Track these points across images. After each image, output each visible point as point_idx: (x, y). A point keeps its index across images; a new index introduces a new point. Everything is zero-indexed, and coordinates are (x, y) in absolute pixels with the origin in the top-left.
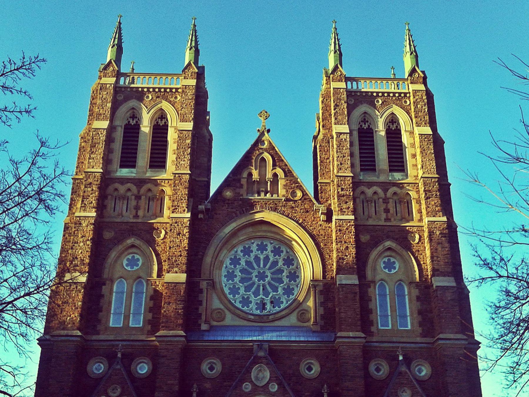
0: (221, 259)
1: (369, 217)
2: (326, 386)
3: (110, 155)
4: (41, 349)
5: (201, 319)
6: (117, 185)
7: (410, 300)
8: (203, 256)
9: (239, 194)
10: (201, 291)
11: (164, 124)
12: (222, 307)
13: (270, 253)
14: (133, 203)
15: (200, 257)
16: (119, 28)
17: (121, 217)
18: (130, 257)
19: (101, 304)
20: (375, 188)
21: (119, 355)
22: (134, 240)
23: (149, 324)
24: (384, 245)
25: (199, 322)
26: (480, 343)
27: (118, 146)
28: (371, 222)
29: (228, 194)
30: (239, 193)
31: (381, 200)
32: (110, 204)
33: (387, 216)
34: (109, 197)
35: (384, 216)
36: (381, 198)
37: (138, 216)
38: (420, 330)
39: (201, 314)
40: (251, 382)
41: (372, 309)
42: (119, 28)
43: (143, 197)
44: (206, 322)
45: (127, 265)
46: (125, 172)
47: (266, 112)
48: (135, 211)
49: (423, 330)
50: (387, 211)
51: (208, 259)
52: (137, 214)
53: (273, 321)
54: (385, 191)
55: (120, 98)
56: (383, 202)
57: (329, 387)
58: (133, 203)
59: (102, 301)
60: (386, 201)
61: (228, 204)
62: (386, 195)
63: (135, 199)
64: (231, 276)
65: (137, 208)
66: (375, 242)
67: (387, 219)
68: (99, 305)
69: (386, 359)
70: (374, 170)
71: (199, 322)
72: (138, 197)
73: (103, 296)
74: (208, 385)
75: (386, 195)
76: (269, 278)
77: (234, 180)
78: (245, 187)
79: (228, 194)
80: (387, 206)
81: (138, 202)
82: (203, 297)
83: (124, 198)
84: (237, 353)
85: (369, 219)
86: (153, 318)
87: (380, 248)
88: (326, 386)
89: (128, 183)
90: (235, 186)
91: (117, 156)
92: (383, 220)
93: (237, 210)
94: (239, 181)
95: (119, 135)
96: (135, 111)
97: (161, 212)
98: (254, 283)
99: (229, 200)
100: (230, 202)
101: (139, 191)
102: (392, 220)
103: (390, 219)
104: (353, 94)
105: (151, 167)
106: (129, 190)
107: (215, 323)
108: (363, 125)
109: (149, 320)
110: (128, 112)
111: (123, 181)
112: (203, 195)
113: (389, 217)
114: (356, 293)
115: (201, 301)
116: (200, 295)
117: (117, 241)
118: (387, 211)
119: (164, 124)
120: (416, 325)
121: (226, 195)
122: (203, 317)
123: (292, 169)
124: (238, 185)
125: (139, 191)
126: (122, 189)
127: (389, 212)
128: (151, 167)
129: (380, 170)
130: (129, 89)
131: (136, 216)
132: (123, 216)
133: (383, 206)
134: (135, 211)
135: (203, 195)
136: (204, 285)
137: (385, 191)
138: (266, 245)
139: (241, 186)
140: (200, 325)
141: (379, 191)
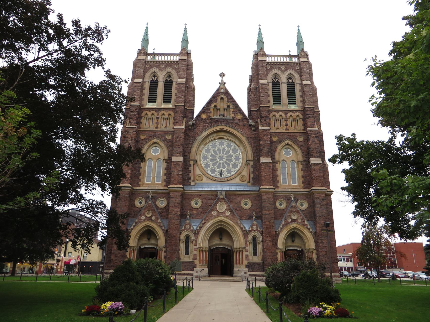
6: (147, 112)
7: (298, 170)
8: (191, 148)
10: (190, 166)
15: (189, 148)
18: (154, 148)
27: (146, 92)
32: (143, 121)
33: (287, 127)
34: (143, 118)
35: (285, 127)
39: (191, 177)
43: (160, 118)
44: (194, 181)
45: (153, 152)
46: (150, 105)
50: (287, 125)
51: (194, 150)
52: (157, 126)
54: (286, 114)
59: (141, 170)
62: (286, 116)
63: (156, 119)
68: (139, 172)
70: (280, 104)
73: (141, 168)
75: (286, 116)
79: (204, 116)
82: (191, 169)
83: (150, 118)
84: (209, 196)
94: (209, 109)
95: (147, 86)
96: (155, 73)
99: (204, 119)
100: (205, 120)
101: (158, 115)
106: (153, 114)
109: (165, 180)
111: (150, 109)
113: (288, 128)
115: (191, 171)
118: (287, 125)
122: (192, 179)
125: (158, 115)
133: (285, 122)
137: (286, 114)
139: (211, 112)
140: (190, 183)
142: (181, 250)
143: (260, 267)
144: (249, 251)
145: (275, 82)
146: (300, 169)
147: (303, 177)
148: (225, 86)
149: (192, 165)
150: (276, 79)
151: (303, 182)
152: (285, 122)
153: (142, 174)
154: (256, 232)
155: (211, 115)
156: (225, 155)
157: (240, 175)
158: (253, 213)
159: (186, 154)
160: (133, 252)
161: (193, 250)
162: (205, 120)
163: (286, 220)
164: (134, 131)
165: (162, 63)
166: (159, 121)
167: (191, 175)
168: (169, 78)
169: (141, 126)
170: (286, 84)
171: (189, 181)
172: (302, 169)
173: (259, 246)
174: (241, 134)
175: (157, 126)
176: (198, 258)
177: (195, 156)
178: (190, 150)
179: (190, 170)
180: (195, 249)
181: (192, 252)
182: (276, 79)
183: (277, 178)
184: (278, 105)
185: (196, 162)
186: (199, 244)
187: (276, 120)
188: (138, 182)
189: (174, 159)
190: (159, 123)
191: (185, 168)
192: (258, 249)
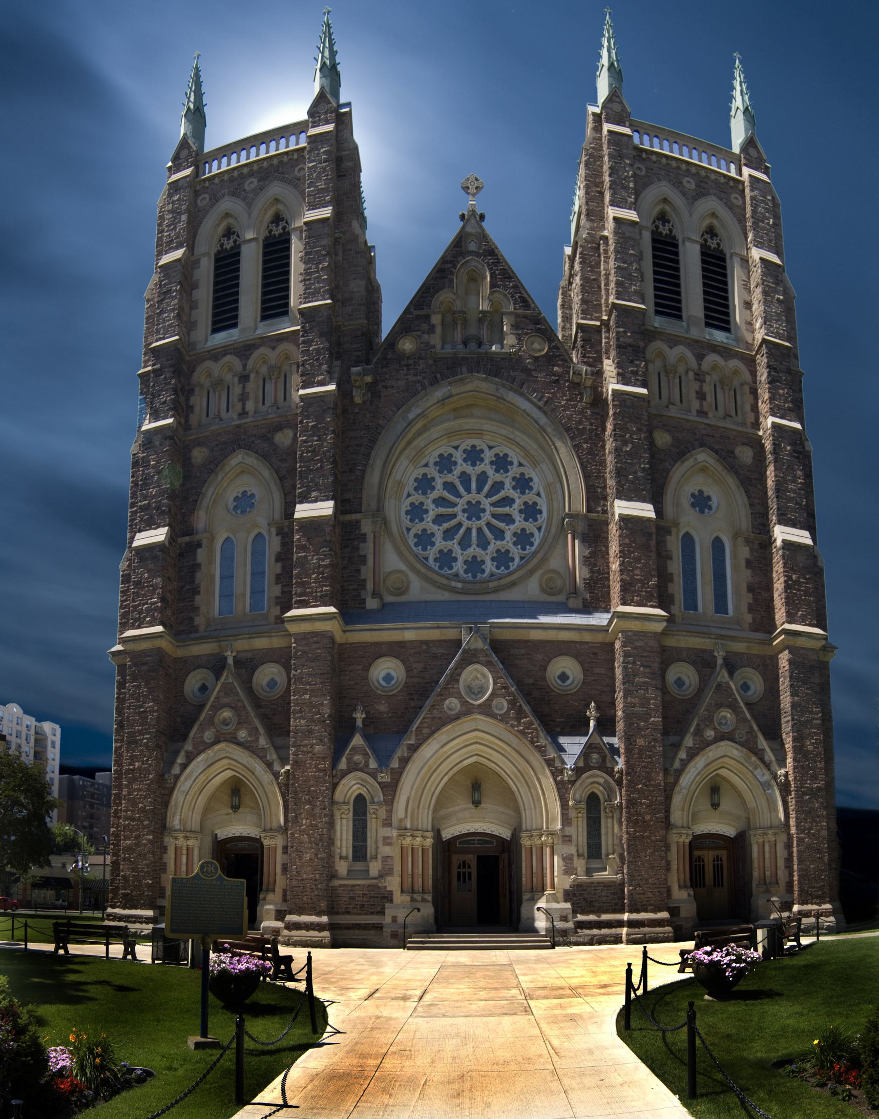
0: (398, 478)
1: (671, 403)
2: (593, 704)
3: (194, 312)
4: (624, 1003)
5: (365, 589)
7: (735, 568)
8: (363, 472)
9: (428, 346)
10: (363, 538)
11: (281, 231)
12: (403, 567)
13: (488, 467)
14: (237, 390)
15: (358, 473)
16: (197, 75)
17: (217, 420)
19: (197, 582)
20: (681, 349)
21: (230, 661)
22: (243, 458)
23: (277, 603)
24: (696, 459)
25: (363, 597)
26: (836, 648)
27: (205, 294)
28: (673, 412)
29: (407, 345)
30: (428, 343)
31: (691, 374)
32: (198, 401)
33: (701, 405)
34: (197, 390)
35: (696, 404)
36: (693, 370)
37: (247, 413)
38: (748, 618)
39: (365, 580)
40: (459, 696)
41: (672, 574)
42: (197, 75)
43: (252, 376)
44: (375, 594)
46: (222, 338)
47: (477, 179)
48: (241, 403)
49: (754, 618)
50: (701, 396)
51: (373, 477)
52: (243, 409)
53: (496, 590)
54: (700, 358)
55: (204, 200)
56: (696, 379)
57: (598, 708)
58: (237, 390)
59: (198, 575)
60: (700, 377)
61: (407, 365)
62: (700, 365)
63: (240, 382)
64: (417, 512)
65: (243, 398)
66: (681, 451)
67: (702, 413)
68: (194, 582)
69: (693, 663)
70: (680, 317)
71: (363, 597)
72: (244, 378)
73: (199, 566)
74: (382, 707)
75: (700, 365)
76: (488, 512)
77: (418, 317)
78: (439, 330)
79: (407, 345)
80: (701, 387)
81: (244, 387)
82: (368, 548)
84: (434, 650)
85: (671, 407)
86: (283, 592)
87: (689, 463)
88: (593, 704)
89: (225, 355)
90: (418, 331)
91: (204, 313)
92: (694, 413)
93: (424, 378)
94: (427, 318)
95: (206, 271)
96: (231, 220)
97: (285, 399)
98: (460, 525)
99: (408, 358)
100: (411, 361)
101: (245, 366)
102: (710, 415)
103: (706, 413)
104: (644, 155)
105: (264, 318)
107: (390, 599)
108: (661, 226)
109: (277, 598)
110: (218, 225)
111: (215, 355)
112: (360, 353)
113: (705, 409)
114: (650, 534)
115: (365, 556)
116: (362, 545)
117: (214, 465)
118: (701, 396)
119: (281, 231)
120: (744, 608)
121: (404, 350)
122: (370, 586)
123: (529, 295)
124: (425, 326)
125: (245, 366)
126: (215, 368)
127: (705, 399)
128: (264, 318)
129: (689, 317)
130: (217, 180)
131: (243, 413)
132: (221, 420)
133: (696, 386)
134: (241, 403)
135: (360, 353)
136: (367, 527)
137: (700, 358)
138: (466, 572)
139: (432, 329)
140: (363, 601)
141: (689, 355)
142: (338, 843)
143: (613, 893)
144: (574, 842)
145: (661, 233)
146: (743, 563)
147: (750, 589)
148: (481, 227)
149: (370, 537)
150: (664, 225)
151: (751, 609)
152: (696, 386)
153: (202, 589)
154: (597, 776)
155: (435, 339)
156: (486, 497)
157: (539, 573)
158: (587, 706)
159: (348, 496)
160: (534, 870)
161: (380, 844)
162: (411, 361)
163: (698, 732)
164: (166, 438)
165: (251, 174)
166: (251, 386)
167: (367, 572)
168: (277, 226)
169: (193, 419)
170: (697, 248)
171: (359, 595)
172: (749, 563)
173: (610, 825)
174: (545, 413)
175: (243, 409)
176: (397, 868)
177: (380, 500)
178: (361, 480)
179: (362, 553)
180: (385, 839)
181: (377, 848)
182: (664, 225)
183: (670, 585)
184: (673, 321)
185: (379, 513)
186: (401, 820)
187: (667, 372)
188: (191, 619)
189: (303, 511)
190: (251, 396)
191: (347, 547)
192: (607, 834)
